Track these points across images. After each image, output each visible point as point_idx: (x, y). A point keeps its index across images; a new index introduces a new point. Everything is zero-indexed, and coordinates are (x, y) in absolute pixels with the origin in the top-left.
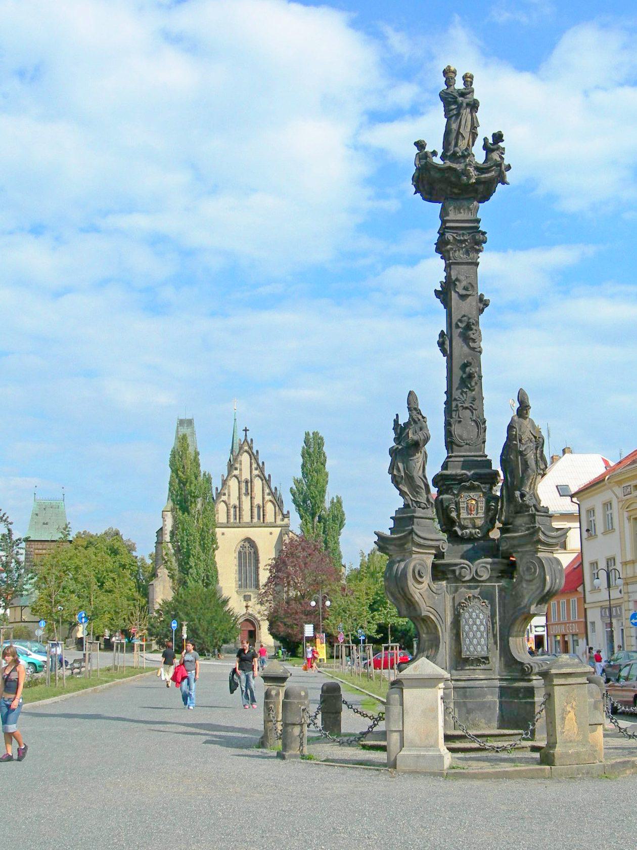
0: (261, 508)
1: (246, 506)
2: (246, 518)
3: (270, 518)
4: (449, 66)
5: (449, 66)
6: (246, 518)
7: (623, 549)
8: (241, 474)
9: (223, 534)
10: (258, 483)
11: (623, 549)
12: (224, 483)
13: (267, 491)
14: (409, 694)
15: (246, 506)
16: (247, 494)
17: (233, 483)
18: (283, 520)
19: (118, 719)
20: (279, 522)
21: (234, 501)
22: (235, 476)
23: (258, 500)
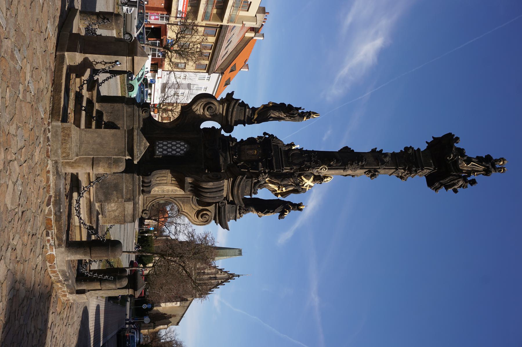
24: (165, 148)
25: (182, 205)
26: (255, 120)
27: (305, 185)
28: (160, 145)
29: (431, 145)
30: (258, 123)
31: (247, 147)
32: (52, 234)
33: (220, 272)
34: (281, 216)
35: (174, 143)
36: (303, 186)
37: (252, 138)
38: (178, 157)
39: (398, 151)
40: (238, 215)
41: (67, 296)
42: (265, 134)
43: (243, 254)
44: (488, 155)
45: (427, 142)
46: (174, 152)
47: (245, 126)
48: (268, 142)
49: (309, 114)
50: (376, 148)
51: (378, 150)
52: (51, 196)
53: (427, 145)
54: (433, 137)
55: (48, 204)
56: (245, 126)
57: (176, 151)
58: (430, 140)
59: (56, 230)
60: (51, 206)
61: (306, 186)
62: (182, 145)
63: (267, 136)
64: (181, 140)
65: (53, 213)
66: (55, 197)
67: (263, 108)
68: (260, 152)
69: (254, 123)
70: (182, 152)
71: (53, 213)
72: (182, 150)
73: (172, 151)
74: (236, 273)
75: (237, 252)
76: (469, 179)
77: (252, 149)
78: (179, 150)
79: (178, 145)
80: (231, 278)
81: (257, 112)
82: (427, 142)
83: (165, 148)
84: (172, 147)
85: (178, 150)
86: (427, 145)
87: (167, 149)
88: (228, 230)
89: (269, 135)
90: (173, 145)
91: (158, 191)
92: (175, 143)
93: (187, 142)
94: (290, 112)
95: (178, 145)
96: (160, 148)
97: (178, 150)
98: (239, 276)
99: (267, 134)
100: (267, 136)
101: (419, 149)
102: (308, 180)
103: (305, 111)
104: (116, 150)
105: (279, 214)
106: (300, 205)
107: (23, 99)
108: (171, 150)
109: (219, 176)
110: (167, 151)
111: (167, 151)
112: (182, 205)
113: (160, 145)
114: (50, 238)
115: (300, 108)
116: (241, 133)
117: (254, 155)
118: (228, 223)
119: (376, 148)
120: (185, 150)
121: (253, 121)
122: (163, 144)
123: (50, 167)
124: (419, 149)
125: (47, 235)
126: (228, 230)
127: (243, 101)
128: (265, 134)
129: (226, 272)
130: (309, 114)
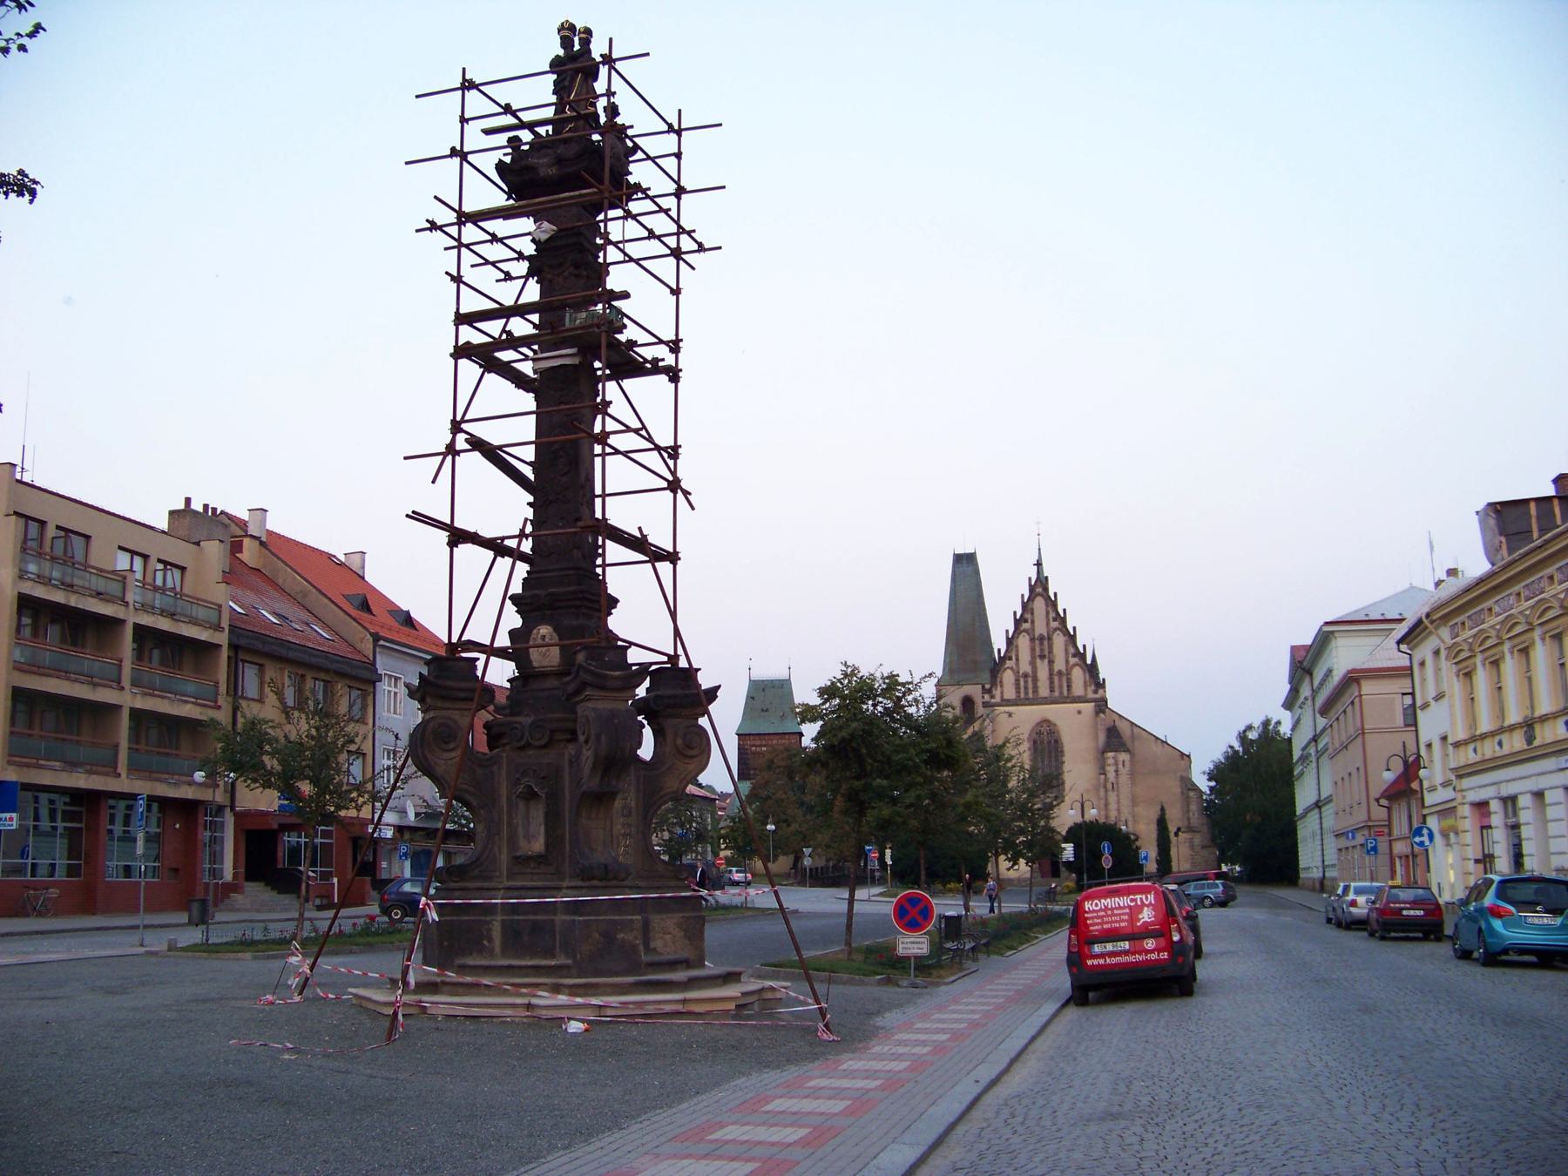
0: (1066, 675)
1: (1043, 674)
2: (1044, 691)
3: (1078, 689)
4: (1294, 649)
5: (1294, 649)
6: (1044, 691)
7: (1453, 724)
8: (1033, 628)
9: (1010, 715)
10: (1059, 641)
11: (1453, 724)
12: (1010, 641)
13: (1072, 650)
14: (186, 591)
15: (1043, 674)
16: (1042, 657)
17: (1023, 642)
18: (1096, 692)
19: (1013, 1062)
20: (1091, 695)
21: (1025, 667)
22: (1025, 631)
23: (1059, 665)
33: (1026, 626)
43: (969, 550)
75: (965, 568)
80: (1046, 589)
98: (1039, 564)
129: (1025, 606)
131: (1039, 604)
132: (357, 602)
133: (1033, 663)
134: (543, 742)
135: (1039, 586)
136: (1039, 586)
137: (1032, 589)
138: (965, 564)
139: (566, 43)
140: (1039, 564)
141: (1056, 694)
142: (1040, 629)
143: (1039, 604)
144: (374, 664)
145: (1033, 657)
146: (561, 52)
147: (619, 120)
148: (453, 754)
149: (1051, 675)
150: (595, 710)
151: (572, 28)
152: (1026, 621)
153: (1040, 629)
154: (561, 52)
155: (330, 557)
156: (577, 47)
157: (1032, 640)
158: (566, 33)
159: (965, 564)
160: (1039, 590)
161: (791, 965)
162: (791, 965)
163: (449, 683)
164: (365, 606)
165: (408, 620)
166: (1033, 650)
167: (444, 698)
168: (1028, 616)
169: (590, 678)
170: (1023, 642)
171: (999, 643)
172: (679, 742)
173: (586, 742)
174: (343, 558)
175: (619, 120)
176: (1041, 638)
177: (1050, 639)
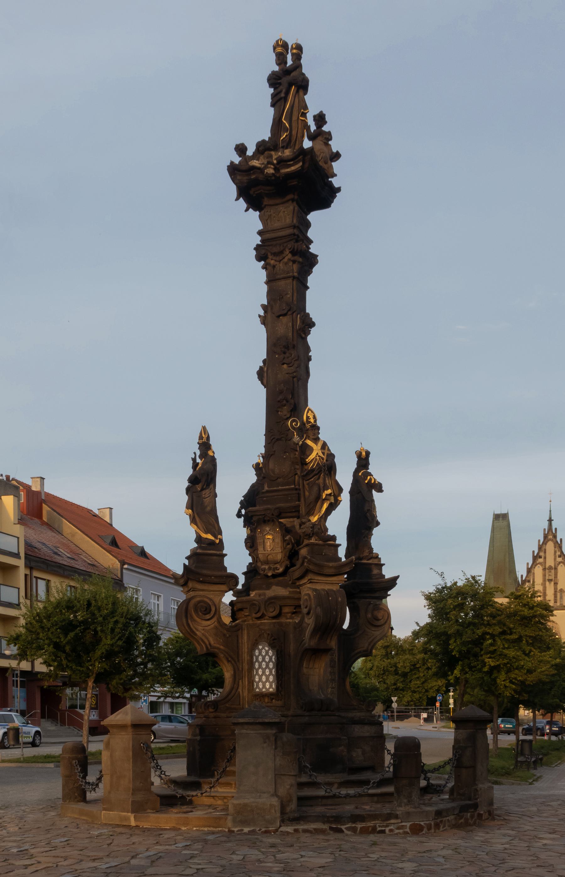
8: (545, 562)
12: (529, 571)
16: (550, 581)
17: (538, 571)
22: (540, 563)
24: (264, 679)
25: (356, 651)
26: (216, 537)
27: (322, 456)
28: (261, 686)
29: (254, 203)
30: (220, 533)
31: (261, 550)
32: (382, 827)
33: (541, 560)
34: (379, 488)
35: (257, 665)
36: (323, 459)
37: (245, 542)
38: (278, 659)
39: (264, 273)
40: (375, 561)
41: (482, 812)
42: (239, 515)
43: (504, 511)
44: (269, 80)
45: (247, 210)
46: (271, 665)
47: (226, 555)
48: (253, 508)
49: (205, 445)
50: (260, 316)
51: (262, 313)
52: (331, 828)
53: (251, 210)
54: (237, 199)
55: (341, 831)
56: (226, 555)
57: (269, 662)
58: (242, 203)
59: (376, 822)
60: (343, 827)
61: (323, 453)
62: (260, 653)
63: (243, 512)
64: (251, 655)
65: (354, 825)
66: (331, 822)
67: (196, 524)
68: (268, 529)
69: (221, 541)
70: (271, 653)
71: (354, 825)
72: (267, 653)
73: (269, 669)
74: (546, 525)
75: (501, 523)
76: (313, 128)
77: (264, 542)
78: (267, 657)
79: (260, 659)
80: (555, 536)
81: (204, 535)
82: (247, 210)
83: (264, 679)
84: (262, 669)
85: (267, 659)
86: (251, 210)
87: (266, 675)
88: (398, 577)
89: (241, 508)
90: (260, 667)
91: (333, 688)
92: (257, 664)
93: (254, 646)
94: (202, 481)
95: (260, 659)
96: (264, 686)
97: (267, 659)
98: (550, 520)
99: (240, 511)
100: (243, 512)
101: (260, 233)
102: (312, 450)
103: (198, 453)
104: (265, 745)
105: (374, 492)
106: (359, 455)
107: (297, 224)
108: (267, 670)
109: (306, 597)
110: (269, 675)
111: (269, 675)
112: (356, 651)
113: (261, 686)
114: (387, 830)
115: (194, 460)
116: (237, 560)
117: (273, 540)
118: (386, 578)
119: (260, 316)
120: (267, 649)
121: (217, 541)
122: (259, 682)
123: (290, 829)
124: (260, 233)
125: (383, 832)
126: (398, 577)
127: (187, 558)
128: (239, 515)
129: (540, 548)
130: (205, 445)
131: (550, 546)
132: (109, 540)
133: (544, 585)
134: (274, 614)
135: (550, 535)
136: (550, 535)
137: (545, 537)
138: (501, 520)
139: (281, 59)
140: (550, 520)
141: (558, 604)
142: (550, 562)
143: (550, 546)
144: (121, 580)
145: (544, 580)
146: (276, 68)
147: (325, 128)
148: (208, 623)
149: (556, 592)
150: (315, 590)
151: (285, 45)
152: (540, 557)
153: (550, 562)
154: (276, 68)
155: (89, 511)
156: (290, 62)
157: (544, 569)
158: (279, 50)
159: (501, 520)
160: (550, 537)
161: (429, 771)
162: (429, 771)
163: (205, 572)
164: (114, 543)
165: (143, 553)
166: (544, 575)
167: (202, 582)
168: (542, 554)
169: (311, 567)
170: (538, 571)
171: (521, 571)
172: (369, 616)
173: (308, 613)
174: (97, 512)
175: (325, 128)
176: (550, 568)
177: (556, 569)
